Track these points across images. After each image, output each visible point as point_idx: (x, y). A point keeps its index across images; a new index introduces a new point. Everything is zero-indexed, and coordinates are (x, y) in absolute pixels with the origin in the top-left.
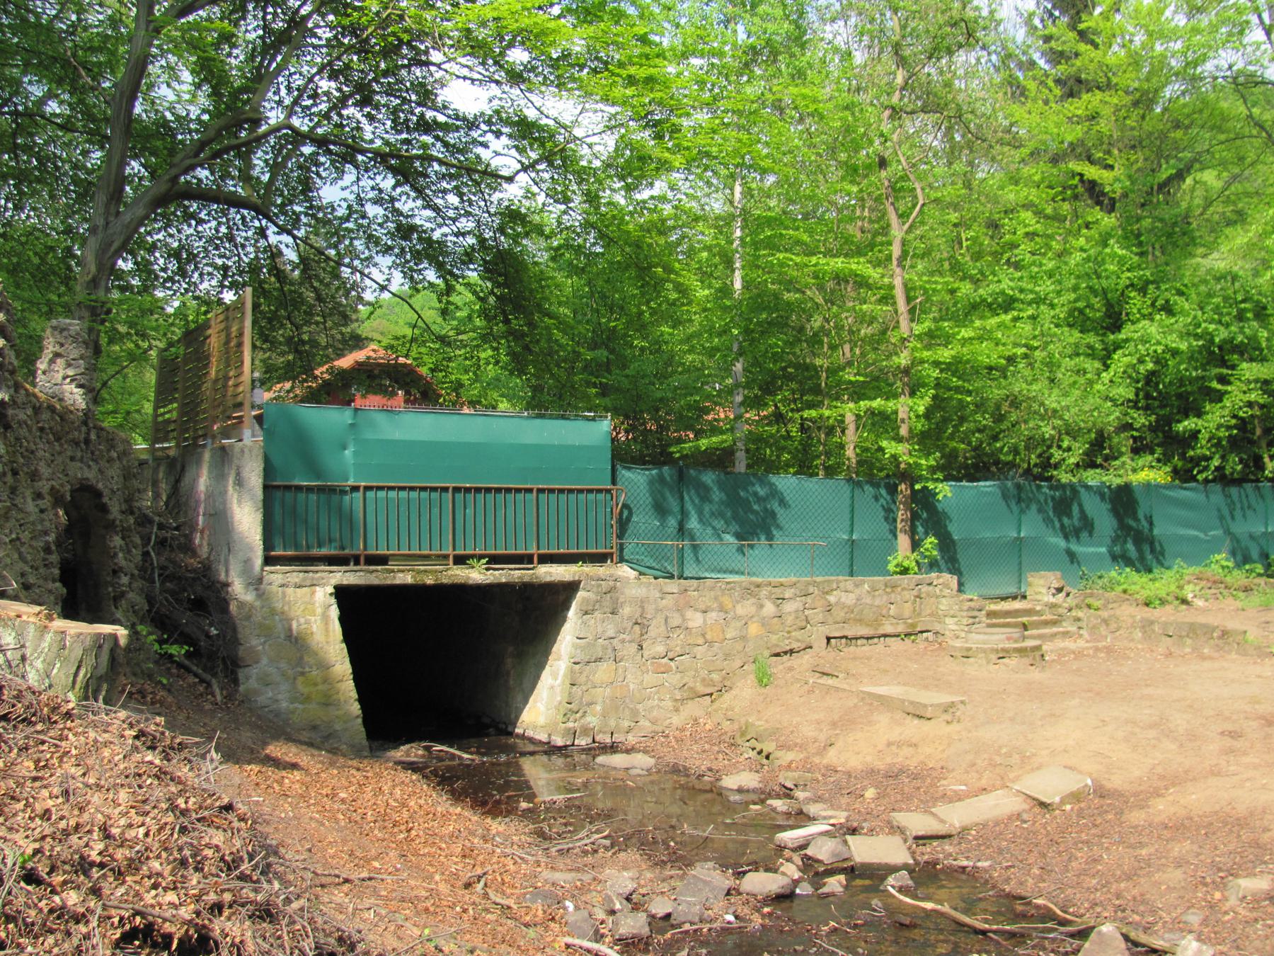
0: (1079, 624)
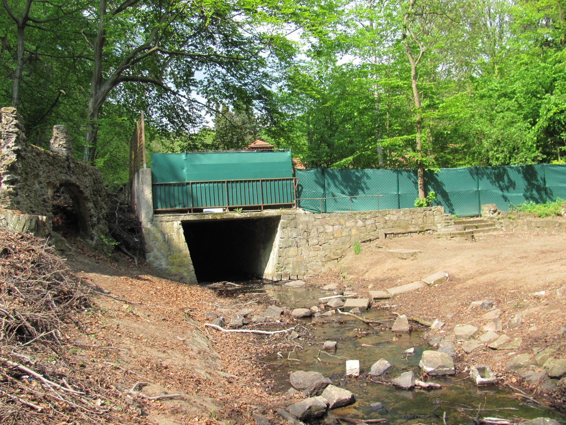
0: (502, 225)
